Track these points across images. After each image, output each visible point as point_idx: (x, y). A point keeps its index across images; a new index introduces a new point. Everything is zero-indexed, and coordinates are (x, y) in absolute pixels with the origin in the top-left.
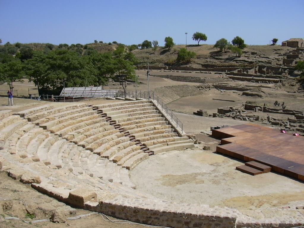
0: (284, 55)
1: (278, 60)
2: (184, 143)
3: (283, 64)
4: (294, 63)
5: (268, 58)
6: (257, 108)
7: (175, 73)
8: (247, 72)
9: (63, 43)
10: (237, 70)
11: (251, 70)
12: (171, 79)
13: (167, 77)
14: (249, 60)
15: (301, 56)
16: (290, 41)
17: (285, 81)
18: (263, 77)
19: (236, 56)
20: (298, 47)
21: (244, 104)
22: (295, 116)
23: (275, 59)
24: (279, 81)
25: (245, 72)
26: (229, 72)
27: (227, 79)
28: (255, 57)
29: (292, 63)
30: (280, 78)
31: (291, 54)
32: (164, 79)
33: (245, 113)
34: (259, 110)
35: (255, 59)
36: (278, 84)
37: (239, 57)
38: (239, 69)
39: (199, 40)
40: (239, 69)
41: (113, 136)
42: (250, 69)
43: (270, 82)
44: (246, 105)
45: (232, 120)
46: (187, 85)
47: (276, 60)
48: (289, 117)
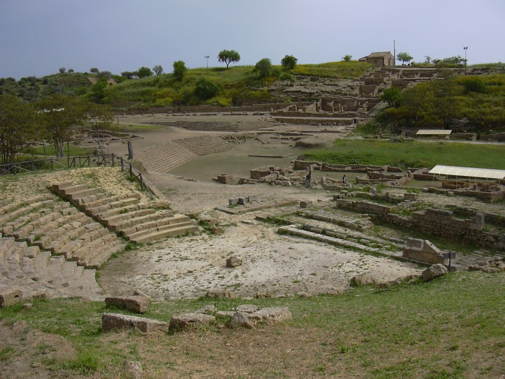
0: (362, 79)
1: (352, 89)
2: (182, 225)
3: (359, 94)
4: (376, 91)
5: (336, 85)
6: (312, 166)
7: (191, 118)
8: (304, 109)
9: (26, 76)
10: (288, 107)
11: (311, 106)
12: (185, 127)
13: (178, 124)
14: (307, 91)
15: (388, 80)
16: (371, 56)
17: (362, 120)
18: (329, 116)
19: (287, 85)
20: (384, 65)
21: (294, 161)
22: (368, 174)
23: (348, 86)
24: (352, 121)
25: (300, 110)
26: (275, 112)
27: (273, 122)
28: (316, 85)
29: (373, 92)
30: (353, 115)
31: (372, 77)
32: (172, 127)
33: (292, 174)
34: (316, 169)
35: (316, 87)
36: (351, 126)
37: (292, 86)
38: (292, 106)
39: (228, 60)
40: (292, 106)
41: (76, 224)
42: (308, 105)
43: (338, 123)
44: (295, 162)
45: (268, 187)
46: (208, 136)
47: (349, 88)
48: (358, 177)
